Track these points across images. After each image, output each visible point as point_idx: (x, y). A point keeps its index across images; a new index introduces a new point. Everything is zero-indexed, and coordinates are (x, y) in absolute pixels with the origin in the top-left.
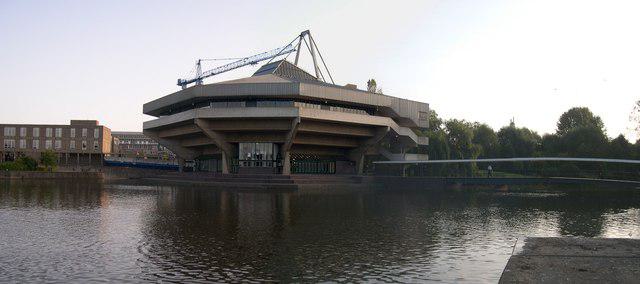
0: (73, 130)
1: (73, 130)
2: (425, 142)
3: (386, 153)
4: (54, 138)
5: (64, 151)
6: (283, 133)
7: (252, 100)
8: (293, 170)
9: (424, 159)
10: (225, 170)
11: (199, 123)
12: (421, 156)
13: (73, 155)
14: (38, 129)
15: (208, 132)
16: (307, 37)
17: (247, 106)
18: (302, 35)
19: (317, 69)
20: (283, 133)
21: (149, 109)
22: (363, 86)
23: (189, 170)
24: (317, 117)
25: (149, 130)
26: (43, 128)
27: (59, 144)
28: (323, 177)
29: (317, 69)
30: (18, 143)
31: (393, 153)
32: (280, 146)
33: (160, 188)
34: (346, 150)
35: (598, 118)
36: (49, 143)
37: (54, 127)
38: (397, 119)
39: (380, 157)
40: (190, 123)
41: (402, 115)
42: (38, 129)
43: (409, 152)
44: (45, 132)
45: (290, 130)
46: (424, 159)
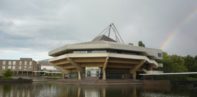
0: (21, 62)
1: (21, 62)
2: (162, 65)
3: (145, 70)
4: (12, 65)
5: (16, 71)
6: (103, 63)
7: (90, 50)
8: (107, 77)
9: (161, 73)
10: (80, 78)
12: (160, 72)
13: (20, 72)
14: (5, 61)
15: (72, 63)
17: (88, 53)
18: (110, 25)
19: (117, 37)
20: (103, 63)
22: (137, 44)
23: (67, 78)
24: (114, 57)
26: (7, 61)
27: (14, 68)
28: (119, 81)
29: (117, 37)
30: (12, 67)
31: (148, 70)
32: (102, 68)
33: (193, 78)
34: (129, 69)
35: (188, 56)
36: (20, 68)
37: (12, 61)
38: (149, 57)
39: (143, 72)
40: (65, 60)
41: (150, 54)
42: (5, 61)
44: (8, 63)
45: (105, 62)
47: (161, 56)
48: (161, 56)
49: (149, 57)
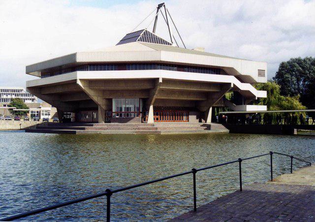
2: (263, 94)
9: (263, 108)
11: (79, 82)
16: (162, 9)
17: (178, 70)
18: (158, 8)
21: (30, 70)
25: (35, 90)
43: (251, 104)
46: (263, 108)
47: (264, 76)
48: (264, 76)
49: (242, 79)
